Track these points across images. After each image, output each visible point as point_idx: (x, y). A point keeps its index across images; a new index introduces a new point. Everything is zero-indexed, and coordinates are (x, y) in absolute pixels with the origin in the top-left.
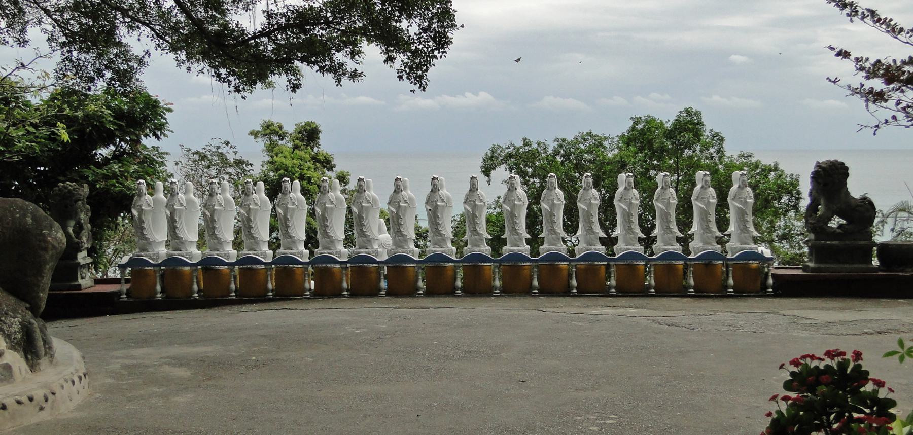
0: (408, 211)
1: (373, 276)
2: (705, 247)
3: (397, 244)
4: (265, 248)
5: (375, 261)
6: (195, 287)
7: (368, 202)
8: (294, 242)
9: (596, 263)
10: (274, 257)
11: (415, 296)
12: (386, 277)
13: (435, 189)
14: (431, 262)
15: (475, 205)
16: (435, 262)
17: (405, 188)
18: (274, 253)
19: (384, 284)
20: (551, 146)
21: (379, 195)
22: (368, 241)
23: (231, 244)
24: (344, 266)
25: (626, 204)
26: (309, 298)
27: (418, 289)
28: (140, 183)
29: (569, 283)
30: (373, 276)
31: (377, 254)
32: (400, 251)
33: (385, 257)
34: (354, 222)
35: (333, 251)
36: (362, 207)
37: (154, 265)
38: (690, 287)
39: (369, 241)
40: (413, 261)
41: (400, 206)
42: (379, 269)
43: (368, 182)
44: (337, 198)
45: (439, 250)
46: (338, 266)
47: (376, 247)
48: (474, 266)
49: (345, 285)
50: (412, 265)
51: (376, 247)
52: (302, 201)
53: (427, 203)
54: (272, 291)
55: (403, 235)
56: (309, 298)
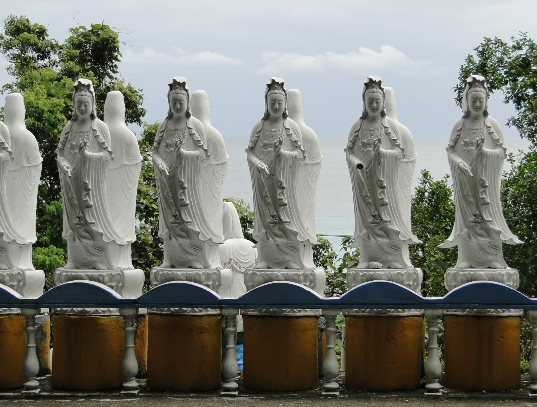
0: (301, 173)
1: (209, 339)
2: (473, 271)
3: (270, 258)
4: (124, 264)
5: (210, 301)
6: (33, 363)
7: (197, 144)
8: (101, 249)
9: (188, 311)
10: (147, 283)
11: (317, 397)
12: (240, 338)
13: (373, 108)
14: (361, 305)
15: (481, 155)
16: (371, 305)
17: (294, 113)
18: (147, 276)
19: (234, 362)
20: (19, 17)
21: (226, 124)
22: (196, 248)
23: (129, 251)
24: (130, 312)
25: (466, 155)
26: (36, 397)
27: (328, 376)
28: (80, 87)
29: (321, 363)
30: (209, 339)
31: (218, 281)
32: (280, 275)
33: (238, 291)
34: (166, 201)
35: (200, 271)
36: (180, 156)
37: (22, 304)
38: (433, 378)
39: (198, 248)
40: (314, 302)
41: (279, 156)
42: (221, 324)
43: (197, 97)
44: (118, 138)
45: (383, 274)
46: (115, 311)
47: (215, 264)
48: (477, 317)
49: (132, 363)
50: (309, 312)
51: (215, 264)
52: (26, 144)
53: (350, 149)
54: (139, 376)
55: (286, 233)
56: (36, 397)
